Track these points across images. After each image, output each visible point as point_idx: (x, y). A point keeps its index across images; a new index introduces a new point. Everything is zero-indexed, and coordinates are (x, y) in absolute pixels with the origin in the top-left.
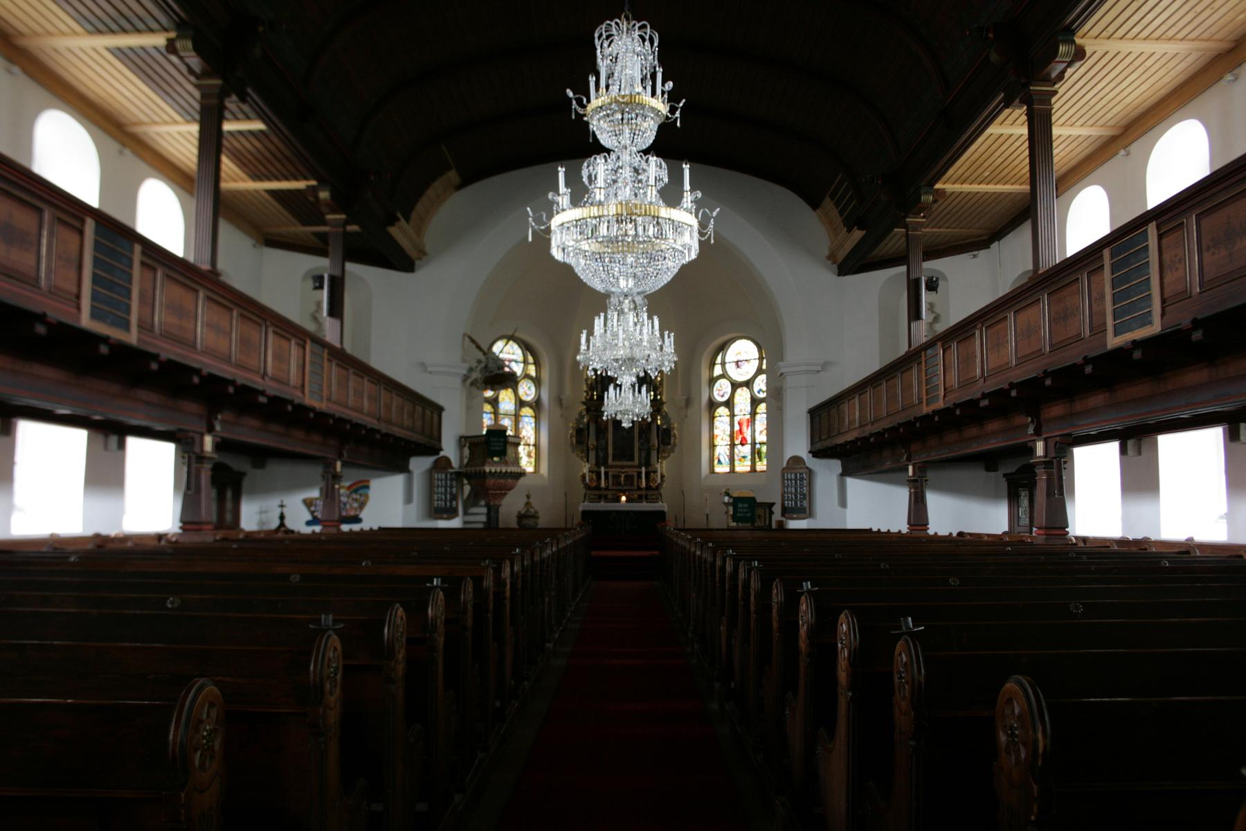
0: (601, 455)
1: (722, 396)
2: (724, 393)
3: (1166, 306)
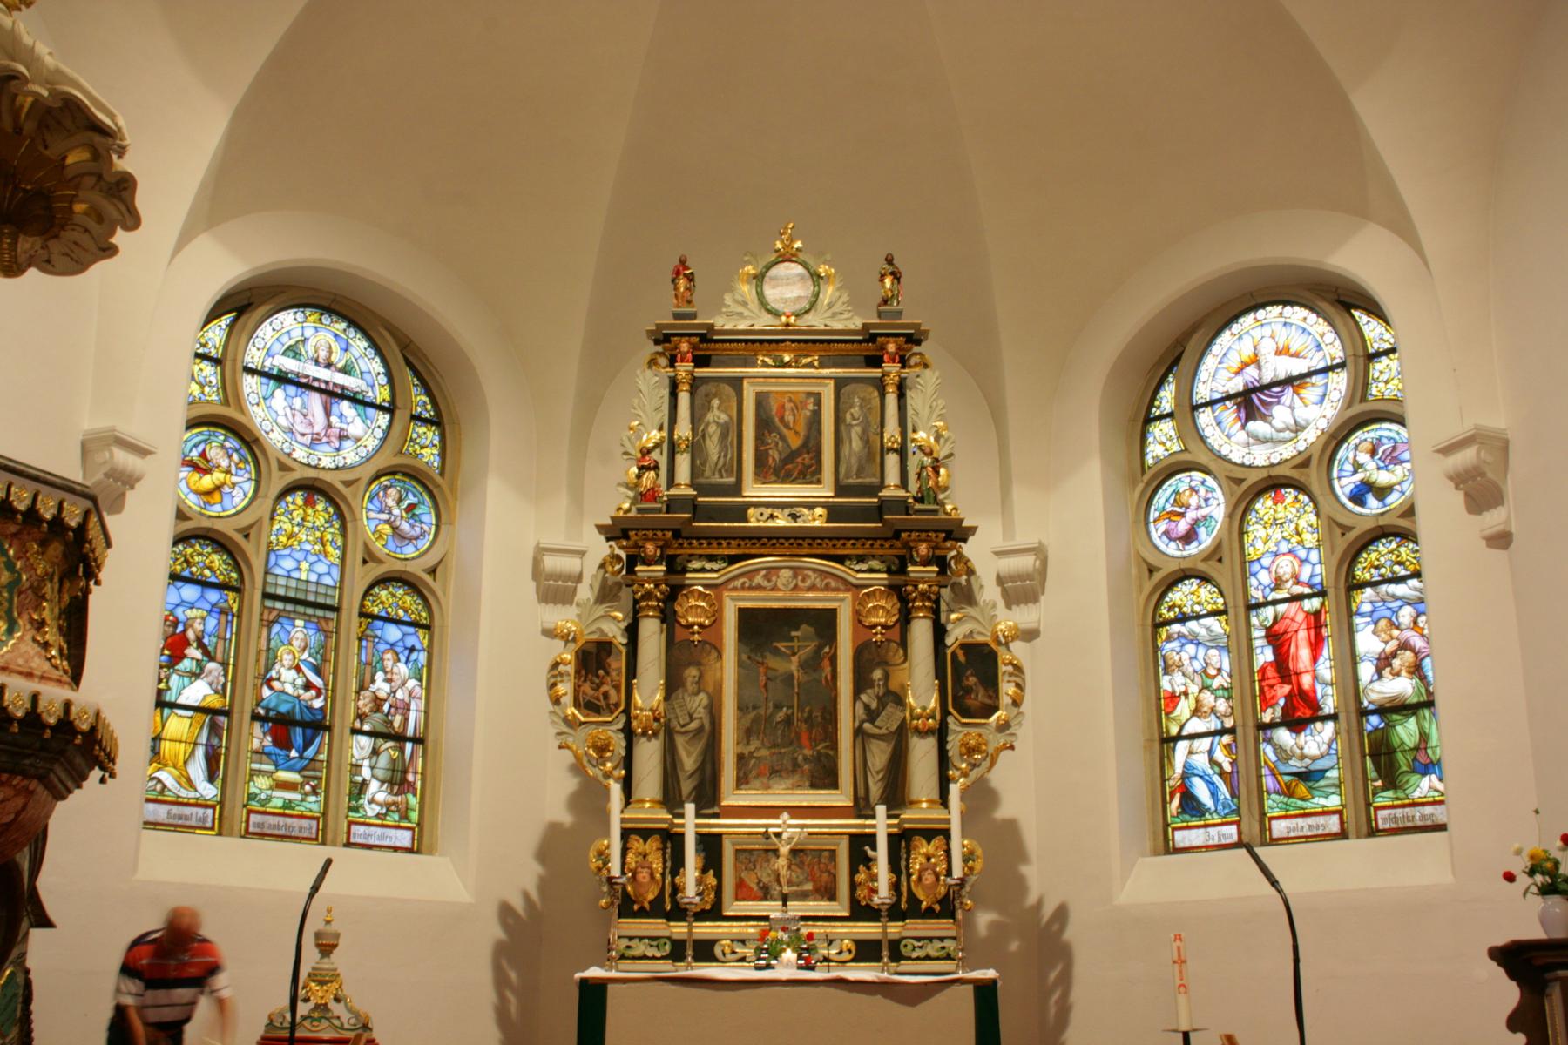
0: (689, 761)
1: (1189, 537)
2: (1195, 523)
3: (757, 940)
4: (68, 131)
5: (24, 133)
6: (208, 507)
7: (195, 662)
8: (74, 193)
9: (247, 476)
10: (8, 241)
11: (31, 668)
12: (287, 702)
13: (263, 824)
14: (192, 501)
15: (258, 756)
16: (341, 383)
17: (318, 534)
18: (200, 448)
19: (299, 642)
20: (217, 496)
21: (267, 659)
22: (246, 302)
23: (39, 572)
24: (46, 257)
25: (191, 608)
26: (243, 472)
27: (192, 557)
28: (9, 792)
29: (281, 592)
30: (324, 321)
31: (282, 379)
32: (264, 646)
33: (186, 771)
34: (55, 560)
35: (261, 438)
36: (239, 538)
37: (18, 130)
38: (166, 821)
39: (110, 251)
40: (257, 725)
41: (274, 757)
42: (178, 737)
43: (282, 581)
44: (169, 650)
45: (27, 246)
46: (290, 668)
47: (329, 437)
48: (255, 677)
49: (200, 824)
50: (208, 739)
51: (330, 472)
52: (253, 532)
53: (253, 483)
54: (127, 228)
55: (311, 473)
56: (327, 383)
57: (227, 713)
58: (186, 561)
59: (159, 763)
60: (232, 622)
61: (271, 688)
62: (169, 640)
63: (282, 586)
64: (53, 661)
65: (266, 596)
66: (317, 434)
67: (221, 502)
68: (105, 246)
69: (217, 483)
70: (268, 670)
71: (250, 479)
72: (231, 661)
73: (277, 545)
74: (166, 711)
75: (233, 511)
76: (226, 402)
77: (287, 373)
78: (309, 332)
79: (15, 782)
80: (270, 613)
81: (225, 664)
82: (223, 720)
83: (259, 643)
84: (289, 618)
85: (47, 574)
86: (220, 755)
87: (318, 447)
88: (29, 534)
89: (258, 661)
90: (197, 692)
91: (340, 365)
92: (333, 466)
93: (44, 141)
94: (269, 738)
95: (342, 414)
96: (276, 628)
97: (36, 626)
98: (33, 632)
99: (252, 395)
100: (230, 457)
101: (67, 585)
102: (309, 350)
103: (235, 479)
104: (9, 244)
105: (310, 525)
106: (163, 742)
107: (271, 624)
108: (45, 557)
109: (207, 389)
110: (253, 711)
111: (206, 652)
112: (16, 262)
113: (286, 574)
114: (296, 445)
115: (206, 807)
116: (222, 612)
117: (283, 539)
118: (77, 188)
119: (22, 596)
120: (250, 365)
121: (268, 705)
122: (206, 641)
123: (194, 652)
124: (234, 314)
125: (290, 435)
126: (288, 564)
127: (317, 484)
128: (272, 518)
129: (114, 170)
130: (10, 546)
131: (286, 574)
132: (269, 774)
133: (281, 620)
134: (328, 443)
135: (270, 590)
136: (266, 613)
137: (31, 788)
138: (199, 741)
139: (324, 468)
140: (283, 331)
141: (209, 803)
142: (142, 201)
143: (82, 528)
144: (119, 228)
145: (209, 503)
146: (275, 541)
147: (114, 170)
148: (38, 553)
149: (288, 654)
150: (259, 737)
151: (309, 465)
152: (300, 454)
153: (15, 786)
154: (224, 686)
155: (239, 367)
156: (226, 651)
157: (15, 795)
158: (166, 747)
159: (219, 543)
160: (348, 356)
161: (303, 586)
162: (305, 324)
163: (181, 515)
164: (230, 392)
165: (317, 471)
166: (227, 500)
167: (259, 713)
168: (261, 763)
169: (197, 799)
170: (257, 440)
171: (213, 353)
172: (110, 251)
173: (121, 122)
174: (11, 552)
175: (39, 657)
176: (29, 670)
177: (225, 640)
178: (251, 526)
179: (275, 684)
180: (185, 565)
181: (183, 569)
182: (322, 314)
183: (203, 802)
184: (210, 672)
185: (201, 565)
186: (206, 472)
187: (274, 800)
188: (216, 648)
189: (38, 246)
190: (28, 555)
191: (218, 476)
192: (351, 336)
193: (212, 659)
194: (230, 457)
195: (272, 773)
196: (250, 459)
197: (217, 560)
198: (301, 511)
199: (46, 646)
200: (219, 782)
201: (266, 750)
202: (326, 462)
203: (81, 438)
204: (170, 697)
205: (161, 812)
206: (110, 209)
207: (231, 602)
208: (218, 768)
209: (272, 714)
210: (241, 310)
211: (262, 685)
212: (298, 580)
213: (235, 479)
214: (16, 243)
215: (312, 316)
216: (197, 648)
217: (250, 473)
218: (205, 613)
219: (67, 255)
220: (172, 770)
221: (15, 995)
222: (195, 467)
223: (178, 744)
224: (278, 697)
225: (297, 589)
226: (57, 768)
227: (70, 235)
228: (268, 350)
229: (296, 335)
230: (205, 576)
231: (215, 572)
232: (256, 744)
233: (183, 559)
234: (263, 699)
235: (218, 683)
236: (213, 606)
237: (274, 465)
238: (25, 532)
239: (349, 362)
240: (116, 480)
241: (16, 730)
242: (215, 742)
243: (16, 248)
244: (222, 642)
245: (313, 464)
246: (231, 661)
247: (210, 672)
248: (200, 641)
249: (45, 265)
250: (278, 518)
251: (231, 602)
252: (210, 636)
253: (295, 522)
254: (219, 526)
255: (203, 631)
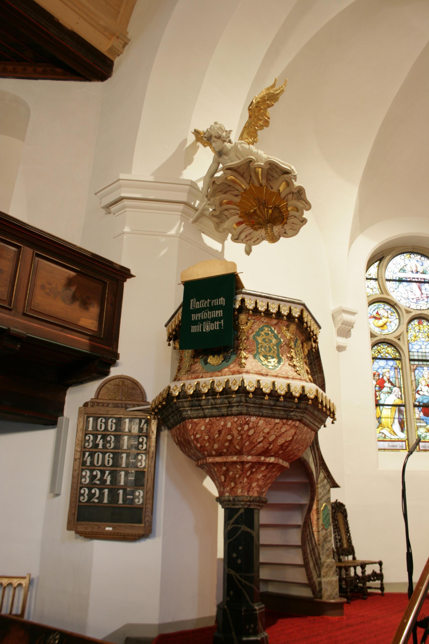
4: (277, 178)
5: (263, 185)
6: (383, 331)
7: (388, 388)
8: (286, 203)
9: (395, 318)
10: (269, 228)
11: (288, 375)
12: (426, 398)
13: (425, 446)
14: (377, 331)
15: (419, 420)
16: (423, 278)
17: (426, 334)
18: (376, 311)
19: (427, 375)
20: (385, 326)
21: (416, 383)
22: (382, 257)
23: (288, 338)
24: (284, 232)
25: (384, 369)
26: (393, 316)
27: (381, 350)
28: (288, 427)
29: (416, 358)
30: (411, 257)
31: (401, 281)
32: (413, 379)
33: (393, 429)
34: (293, 332)
35: (397, 303)
36: (396, 340)
37: (261, 185)
38: (388, 448)
39: (304, 221)
40: (416, 409)
41: (425, 420)
42: (387, 416)
43: (416, 354)
44: (378, 385)
45: (277, 229)
46: (425, 386)
47: (423, 298)
48: (412, 391)
49: (401, 448)
50: (399, 416)
51: (426, 311)
52: (401, 337)
53: (398, 320)
54: (307, 210)
55: (419, 312)
56: (418, 279)
57: (404, 406)
58: (379, 352)
59: (382, 427)
60: (400, 371)
61: (419, 394)
62: (378, 381)
63: (416, 355)
64: (298, 372)
65: (411, 360)
66: (418, 298)
67: (387, 329)
68: (302, 220)
69: (385, 322)
70: (417, 388)
71: (396, 319)
72: (402, 386)
73: (411, 341)
74: (381, 407)
75: (393, 331)
76: (382, 293)
77: (402, 278)
78: (407, 262)
79: (289, 423)
80: (413, 366)
81: (400, 388)
82: (403, 408)
83: (411, 378)
84: (421, 367)
85: (291, 338)
86: (404, 422)
87: (420, 302)
88: (281, 323)
89: (412, 385)
90: (392, 399)
91: (421, 271)
92: (427, 308)
93: (271, 186)
94: (422, 413)
95: (426, 289)
96: (417, 371)
97: (290, 359)
98: (289, 362)
99: (391, 289)
100: (387, 312)
101: (305, 345)
102: (408, 268)
103: (390, 320)
104: (270, 229)
105: (422, 331)
106: (382, 419)
107: (414, 370)
108: (289, 331)
109: (374, 290)
110: (414, 404)
111: (392, 384)
112: (274, 236)
113: (417, 351)
114: (411, 303)
115: (402, 441)
116: (395, 368)
117: (413, 338)
118: (287, 201)
119: (282, 348)
120: (388, 278)
121: (419, 400)
122: (391, 380)
123: (387, 384)
124: (379, 262)
125: (408, 300)
126: (416, 347)
127: (422, 316)
128: (407, 331)
129: (295, 187)
130: (275, 329)
131: (417, 351)
132: (425, 427)
133: (418, 368)
134: (423, 300)
135: (412, 358)
136: (412, 366)
137: (297, 425)
138: (395, 417)
139: (423, 310)
140: (397, 264)
141: (403, 440)
142: (309, 196)
143: (301, 318)
144: (304, 210)
145: (383, 330)
146: (410, 340)
147: (295, 187)
148: (286, 330)
149: (423, 380)
150: (418, 413)
151: (417, 310)
152: (413, 306)
153: (290, 425)
154: (401, 396)
155: (384, 280)
156: (399, 383)
157: (291, 428)
158: (383, 420)
159: (390, 344)
160: (423, 267)
161: (424, 354)
162: (405, 260)
163: (372, 336)
164: (383, 289)
165: (420, 311)
166: (389, 327)
167: (416, 404)
168: (420, 423)
169: (398, 439)
170: (396, 304)
171: (374, 277)
172: (304, 221)
173: (293, 167)
174: (276, 332)
175: (292, 371)
176: (287, 376)
177: (398, 378)
178: (400, 335)
179: (420, 392)
180: (378, 353)
181: (378, 355)
182: (410, 255)
183: (401, 440)
184: (395, 391)
185: (384, 352)
186: (380, 319)
187: (428, 436)
188: (395, 382)
189: (280, 228)
190: (282, 331)
191: (384, 320)
192: (423, 260)
193: (395, 386)
194: (387, 312)
195: (425, 426)
196: (395, 311)
197: (390, 350)
198: (418, 327)
199: (294, 366)
200: (405, 432)
201: (422, 418)
202: (424, 307)
203: (331, 313)
204: (381, 402)
205: (385, 445)
206: (300, 204)
207: (398, 364)
208: (404, 426)
209: (421, 404)
210: (381, 260)
211: (415, 393)
212: (422, 352)
213: (390, 320)
214: (273, 229)
215: (407, 256)
216: (389, 383)
217: (396, 316)
218: (389, 370)
219: (292, 229)
220: (387, 429)
221: (328, 514)
222: (376, 318)
223: (387, 419)
224: (422, 397)
225: (422, 356)
226: (305, 415)
227: (290, 221)
228: (393, 271)
229: (403, 264)
230: (387, 356)
231: (390, 354)
232: (417, 416)
233: (377, 351)
234: (417, 399)
235: (399, 395)
236: (392, 367)
237: (404, 312)
238: (280, 323)
239: (425, 270)
240: (346, 325)
241: (282, 400)
242: (401, 417)
243: (273, 230)
244: (397, 379)
245: (419, 309)
246: (402, 386)
247: (395, 391)
248: (389, 380)
249: (285, 235)
250: (409, 331)
251: (398, 364)
252: (392, 378)
253: (416, 331)
254: (388, 337)
255: (390, 377)
